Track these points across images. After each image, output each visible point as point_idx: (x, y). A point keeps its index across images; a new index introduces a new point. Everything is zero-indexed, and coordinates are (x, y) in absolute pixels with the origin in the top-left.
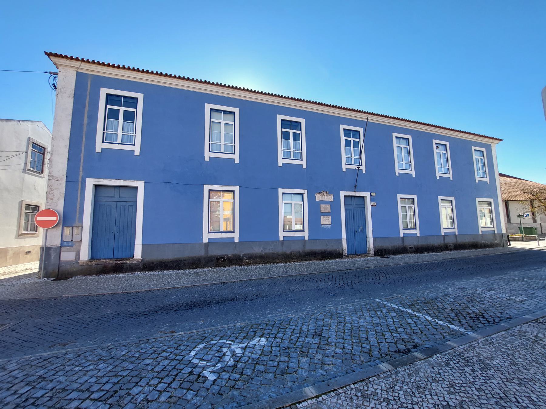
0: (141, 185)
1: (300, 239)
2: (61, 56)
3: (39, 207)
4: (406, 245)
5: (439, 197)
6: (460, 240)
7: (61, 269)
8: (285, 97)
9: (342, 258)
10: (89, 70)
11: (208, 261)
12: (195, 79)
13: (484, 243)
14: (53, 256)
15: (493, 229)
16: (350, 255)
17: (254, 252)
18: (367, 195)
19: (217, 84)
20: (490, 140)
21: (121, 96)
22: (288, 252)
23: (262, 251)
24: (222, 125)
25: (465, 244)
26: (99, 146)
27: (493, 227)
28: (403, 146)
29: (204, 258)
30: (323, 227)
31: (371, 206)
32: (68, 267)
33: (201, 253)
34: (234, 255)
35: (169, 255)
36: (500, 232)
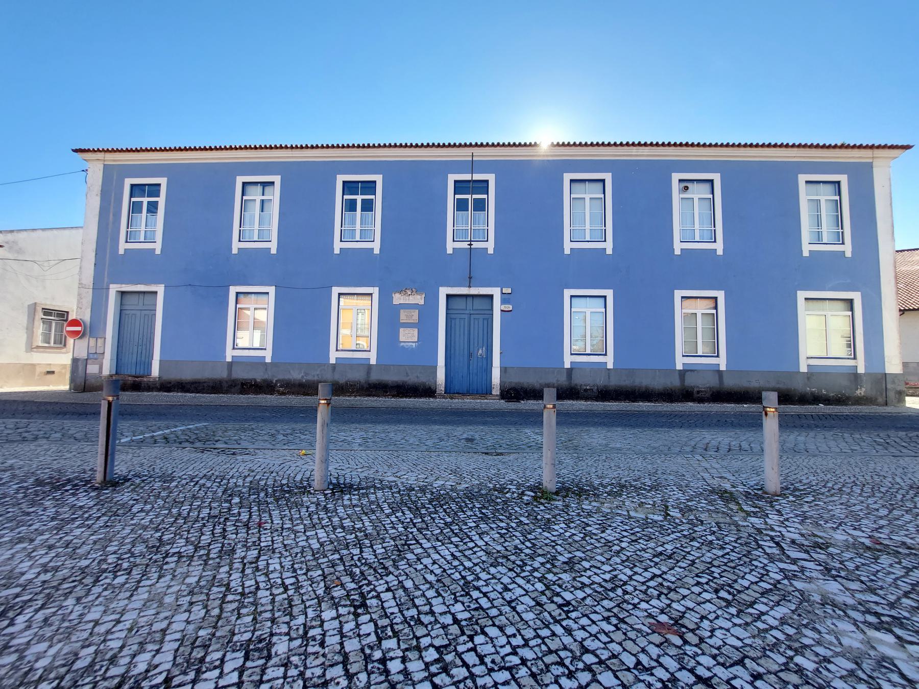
0: (160, 289)
1: (363, 362)
2: (89, 151)
3: (68, 312)
4: (576, 385)
5: (675, 291)
6: (730, 383)
7: (87, 382)
8: (563, 143)
9: (434, 397)
10: (114, 161)
11: (231, 385)
12: (490, 144)
13: (812, 393)
14: (81, 368)
15: (851, 363)
16: (450, 391)
17: (291, 377)
18: (496, 292)
19: (498, 145)
20: (868, 153)
21: (358, 182)
22: (342, 381)
23: (303, 377)
24: (587, 201)
25: (748, 392)
26: (123, 247)
27: (855, 358)
28: (825, 196)
29: (227, 382)
30: (403, 346)
31: (502, 311)
32: (93, 381)
33: (222, 374)
34: (265, 381)
35: (187, 375)
36: (876, 370)
